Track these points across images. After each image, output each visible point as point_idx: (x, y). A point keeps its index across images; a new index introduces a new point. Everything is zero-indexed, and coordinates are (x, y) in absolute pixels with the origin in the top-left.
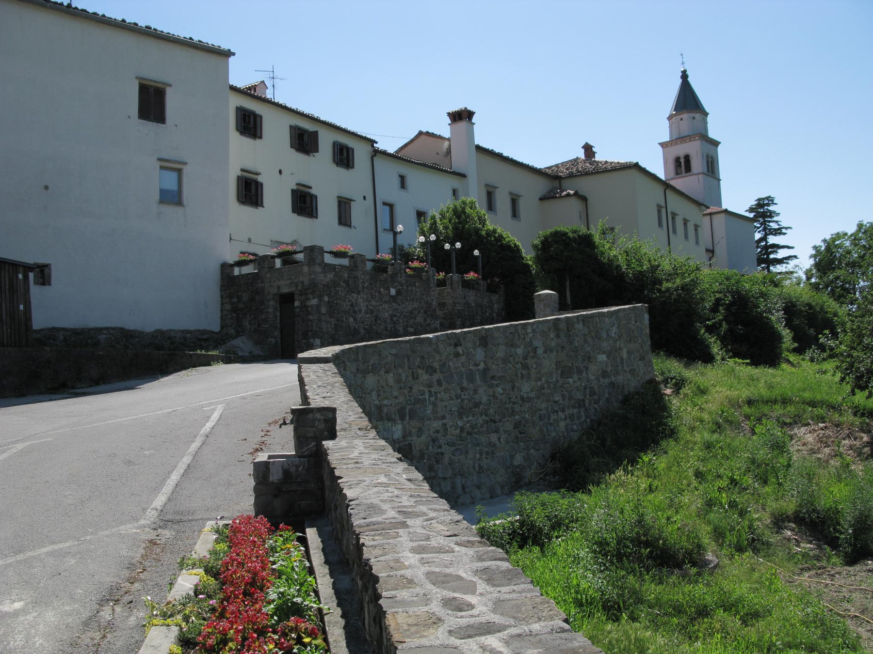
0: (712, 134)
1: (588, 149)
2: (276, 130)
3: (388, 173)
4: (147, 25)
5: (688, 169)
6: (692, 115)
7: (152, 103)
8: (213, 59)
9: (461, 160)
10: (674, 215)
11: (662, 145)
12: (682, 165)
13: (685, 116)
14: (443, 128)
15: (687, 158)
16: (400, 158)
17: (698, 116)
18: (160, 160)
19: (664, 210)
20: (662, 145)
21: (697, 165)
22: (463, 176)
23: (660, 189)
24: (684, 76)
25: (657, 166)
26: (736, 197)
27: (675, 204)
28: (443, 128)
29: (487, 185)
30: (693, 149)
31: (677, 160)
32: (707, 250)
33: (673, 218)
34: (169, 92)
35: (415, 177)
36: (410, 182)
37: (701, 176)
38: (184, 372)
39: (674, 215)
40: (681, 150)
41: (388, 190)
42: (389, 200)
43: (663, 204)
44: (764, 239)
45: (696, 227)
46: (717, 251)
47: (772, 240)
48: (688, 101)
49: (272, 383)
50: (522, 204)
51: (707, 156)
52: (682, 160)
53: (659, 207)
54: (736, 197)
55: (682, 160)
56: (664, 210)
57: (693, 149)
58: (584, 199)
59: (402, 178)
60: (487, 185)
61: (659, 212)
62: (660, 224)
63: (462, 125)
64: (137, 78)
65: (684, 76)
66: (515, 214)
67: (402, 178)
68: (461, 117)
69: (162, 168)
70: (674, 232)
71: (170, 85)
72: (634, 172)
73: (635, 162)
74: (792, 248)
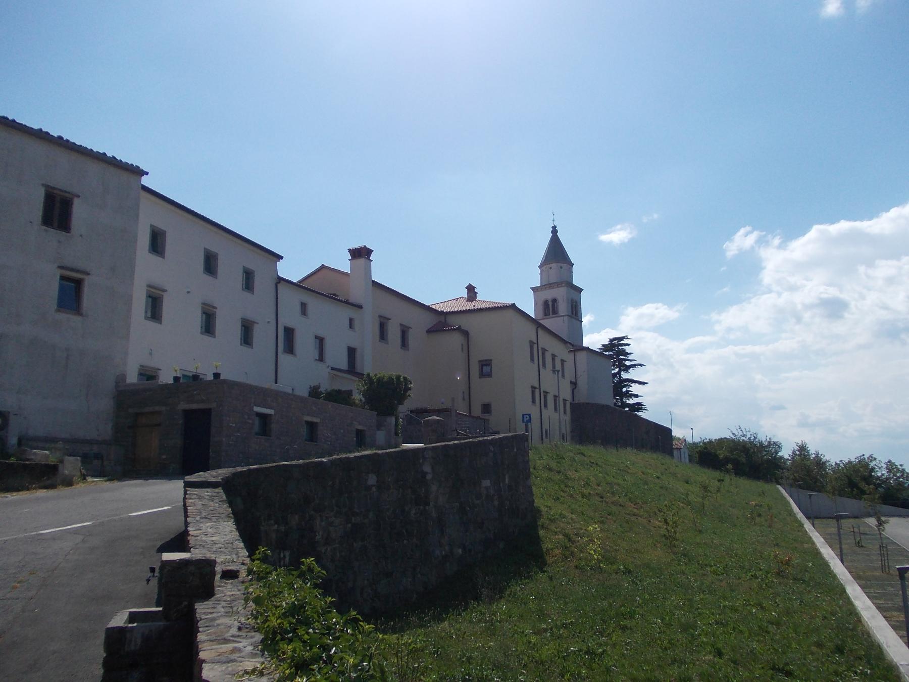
0: (576, 282)
1: (471, 289)
2: (184, 251)
3: (290, 301)
4: (59, 134)
5: (555, 312)
6: (559, 264)
7: (57, 211)
8: (125, 176)
9: (358, 293)
10: (544, 350)
11: (534, 289)
12: (549, 307)
13: (554, 265)
14: (343, 264)
15: (555, 301)
16: (300, 286)
17: (565, 266)
18: (61, 268)
19: (535, 346)
20: (534, 289)
21: (563, 308)
22: (360, 307)
23: (530, 331)
24: (554, 231)
25: (529, 308)
26: (594, 339)
27: (545, 341)
28: (343, 264)
29: (380, 317)
30: (560, 293)
31: (546, 303)
32: (571, 382)
33: (543, 354)
34: (76, 202)
35: (314, 304)
36: (310, 309)
37: (566, 318)
38: (173, 536)
39: (544, 350)
40: (549, 295)
41: (290, 317)
42: (290, 325)
43: (537, 386)
44: (619, 373)
45: (563, 361)
46: (580, 383)
47: (625, 376)
48: (556, 254)
49: (154, 500)
50: (411, 335)
51: (572, 300)
52: (550, 304)
53: (533, 388)
54: (594, 339)
55: (550, 304)
56: (535, 346)
57: (560, 293)
58: (466, 334)
59: (304, 306)
60: (380, 317)
61: (533, 393)
62: (532, 359)
63: (361, 261)
64: (43, 185)
65: (554, 231)
66: (404, 344)
67: (304, 306)
68: (361, 254)
69: (63, 278)
70: (546, 406)
71: (78, 196)
72: (510, 313)
73: (511, 302)
74: (644, 383)
